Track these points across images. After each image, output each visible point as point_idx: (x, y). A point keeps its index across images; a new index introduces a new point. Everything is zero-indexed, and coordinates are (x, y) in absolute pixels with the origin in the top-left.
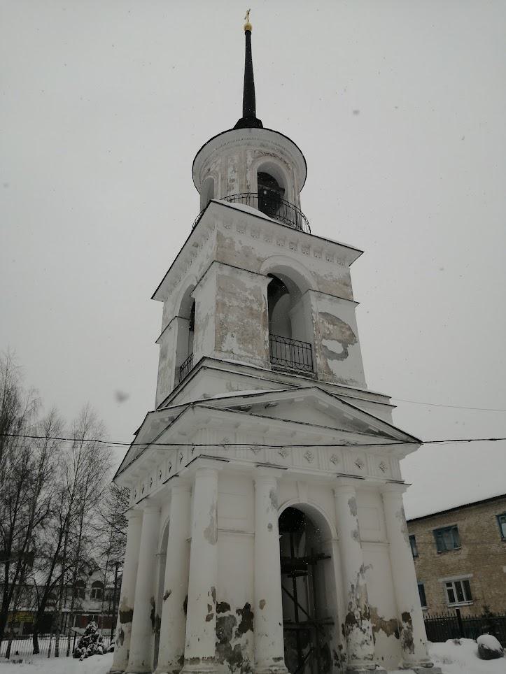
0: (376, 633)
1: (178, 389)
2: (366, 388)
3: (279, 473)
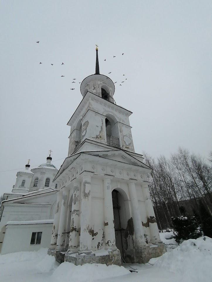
0: (193, 181)
1: (76, 150)
2: (134, 151)
3: (112, 177)
